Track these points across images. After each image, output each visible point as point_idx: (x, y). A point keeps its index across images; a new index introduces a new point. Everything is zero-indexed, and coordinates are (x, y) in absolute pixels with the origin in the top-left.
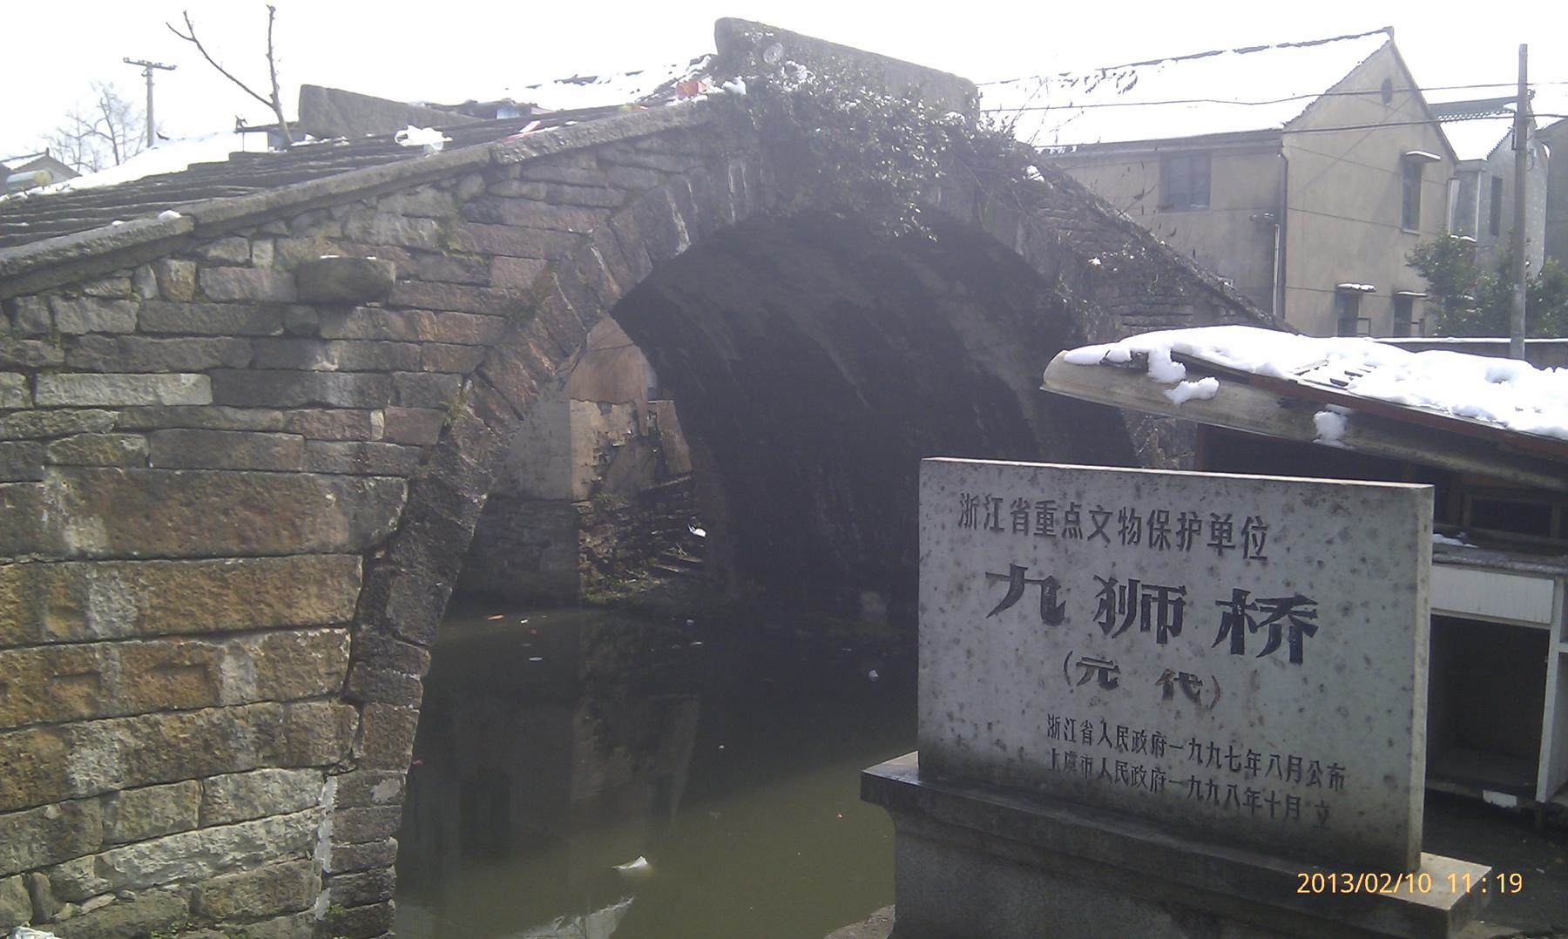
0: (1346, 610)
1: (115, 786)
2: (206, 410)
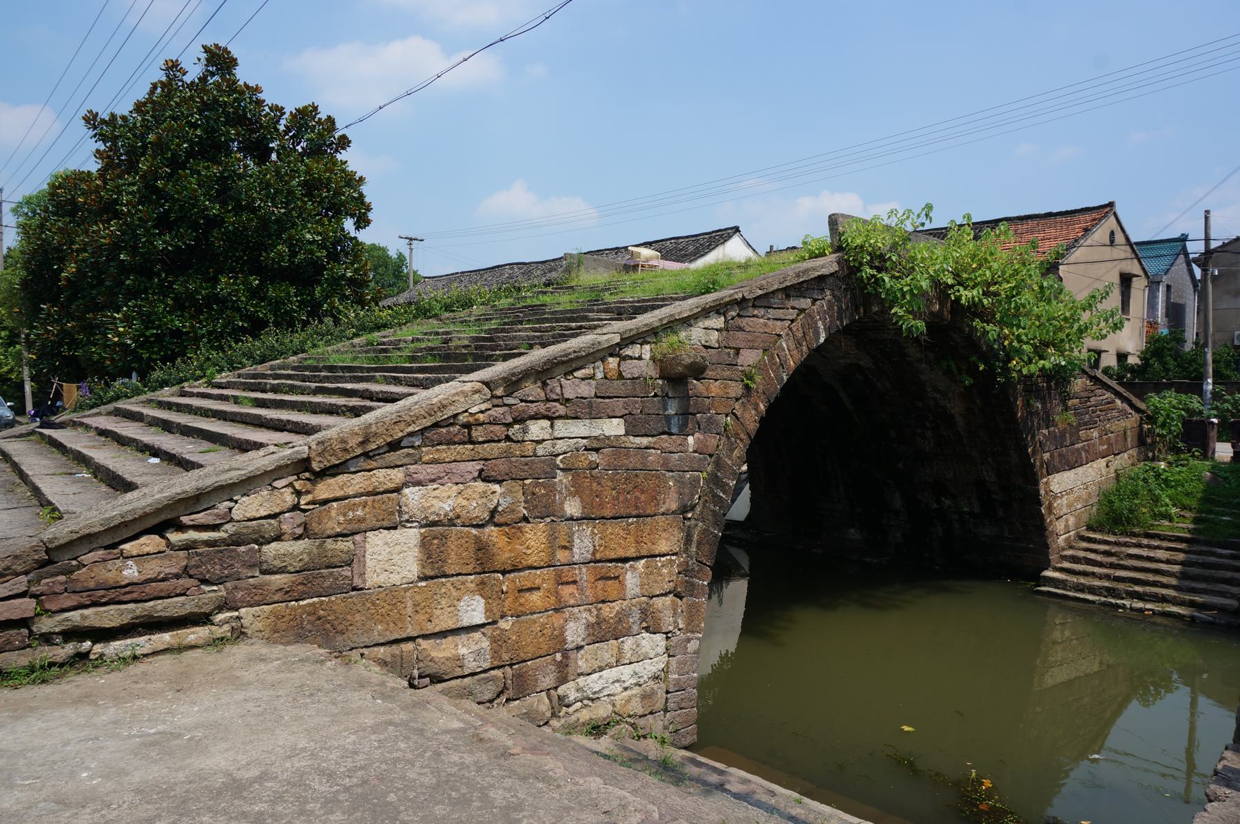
1: (582, 643)
2: (622, 438)
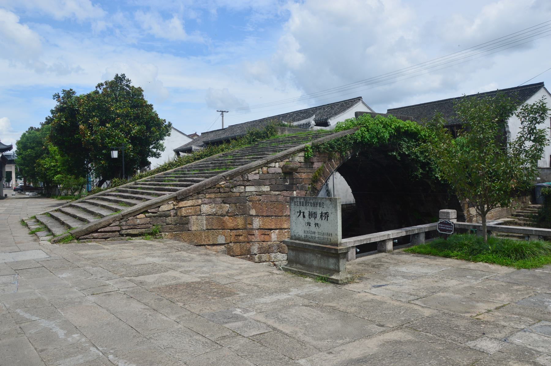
0: (331, 213)
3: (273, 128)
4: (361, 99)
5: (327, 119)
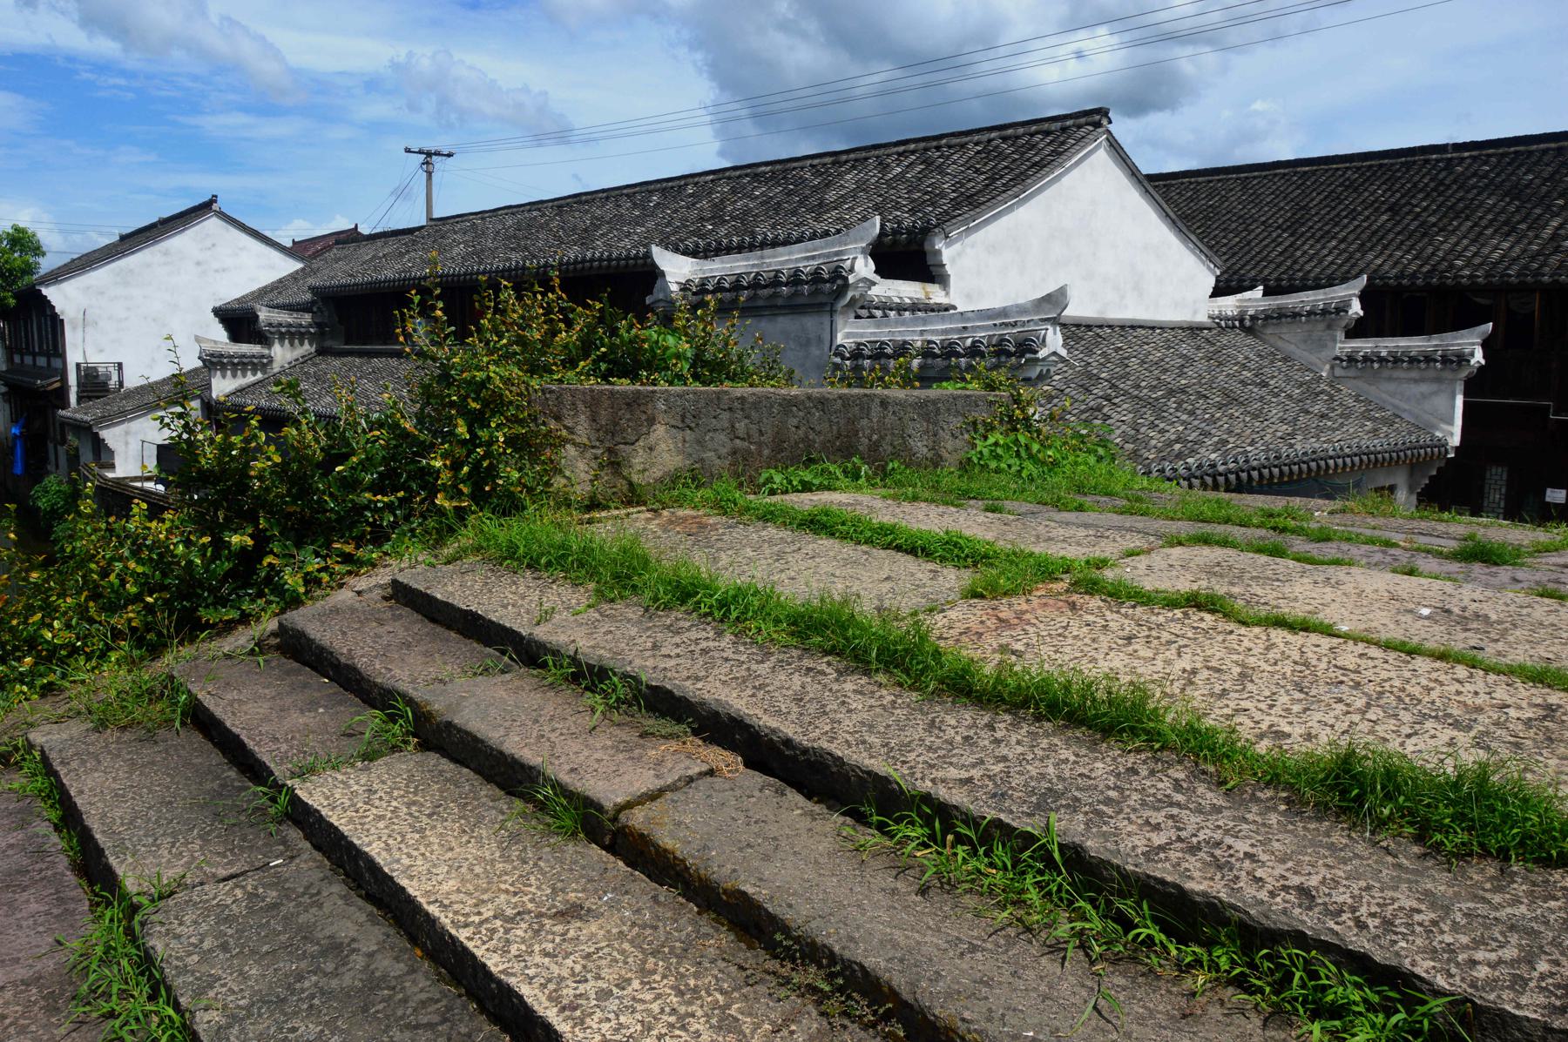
3: (495, 403)
4: (1105, 122)
5: (927, 231)
